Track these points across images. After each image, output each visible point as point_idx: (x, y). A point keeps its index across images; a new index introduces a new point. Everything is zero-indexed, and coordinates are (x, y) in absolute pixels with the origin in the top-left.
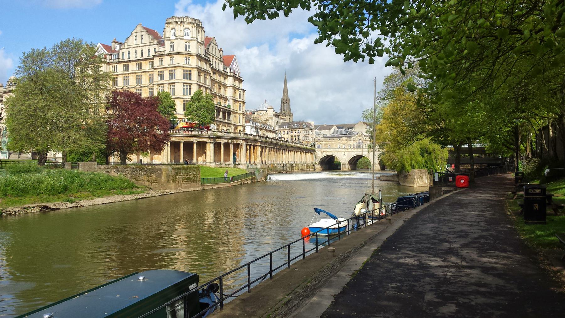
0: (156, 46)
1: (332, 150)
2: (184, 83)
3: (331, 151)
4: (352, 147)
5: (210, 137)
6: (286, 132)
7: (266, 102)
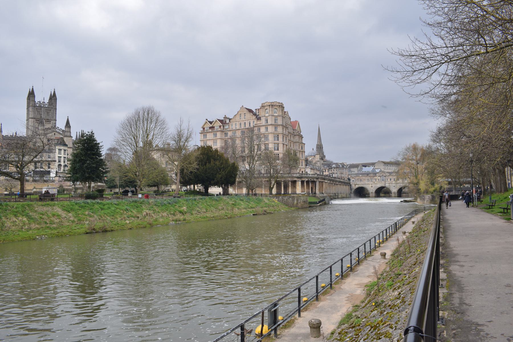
0: (254, 120)
1: (362, 183)
2: (275, 143)
3: (362, 184)
4: (377, 181)
5: (298, 178)
6: (327, 170)
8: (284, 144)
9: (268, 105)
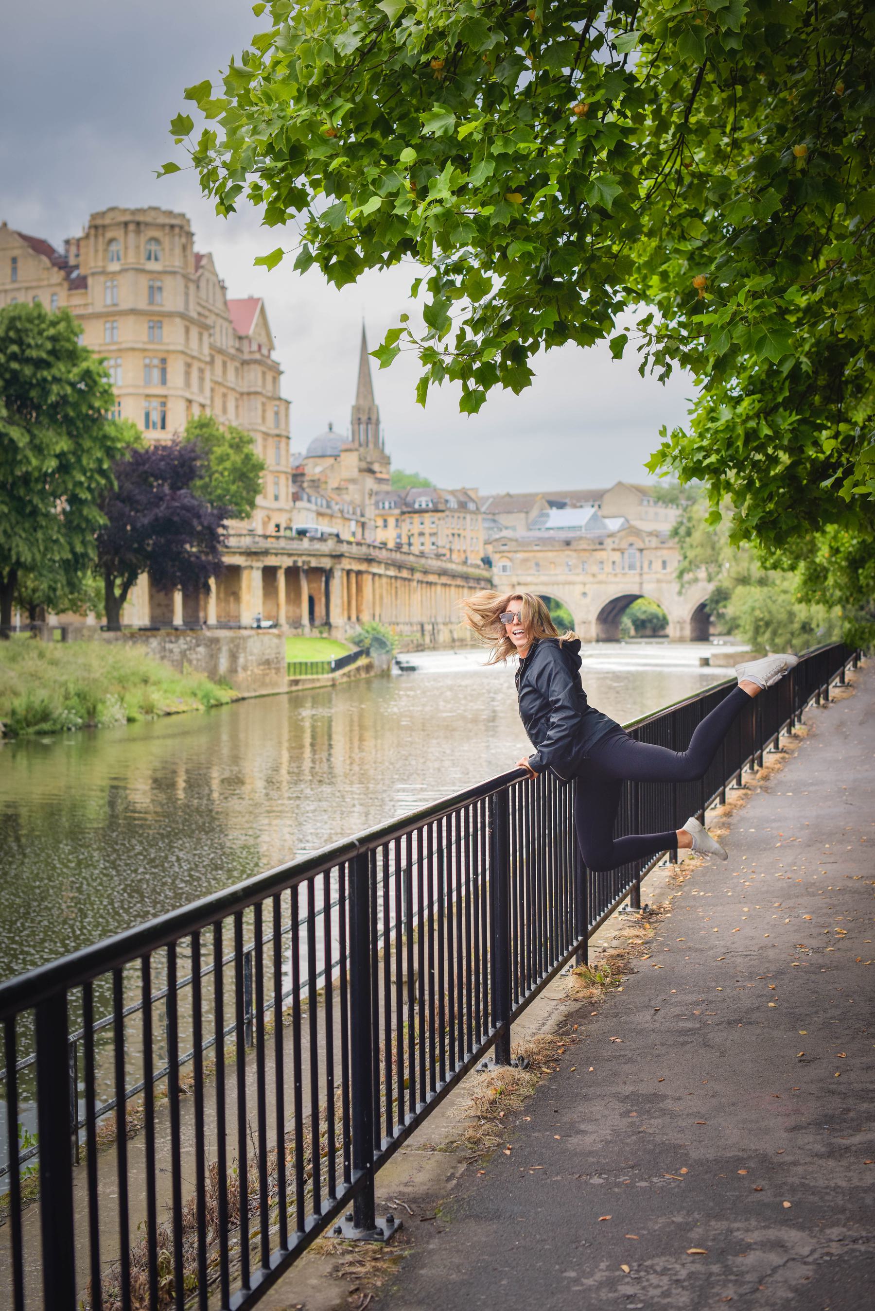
4: (608, 568)
5: (249, 554)
6: (391, 522)
7: (331, 429)
8: (190, 402)
9: (118, 224)
